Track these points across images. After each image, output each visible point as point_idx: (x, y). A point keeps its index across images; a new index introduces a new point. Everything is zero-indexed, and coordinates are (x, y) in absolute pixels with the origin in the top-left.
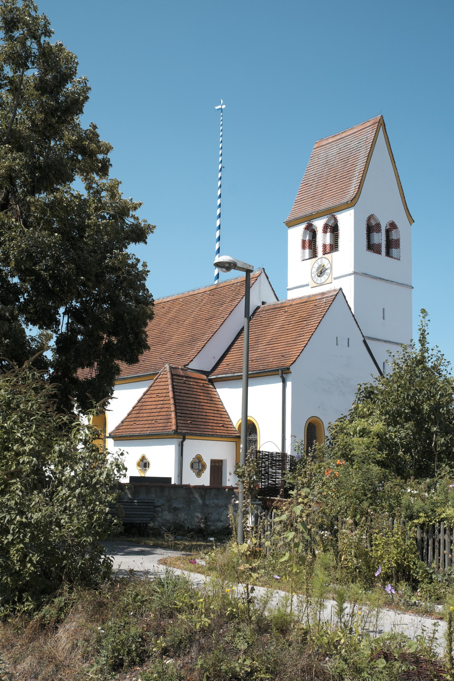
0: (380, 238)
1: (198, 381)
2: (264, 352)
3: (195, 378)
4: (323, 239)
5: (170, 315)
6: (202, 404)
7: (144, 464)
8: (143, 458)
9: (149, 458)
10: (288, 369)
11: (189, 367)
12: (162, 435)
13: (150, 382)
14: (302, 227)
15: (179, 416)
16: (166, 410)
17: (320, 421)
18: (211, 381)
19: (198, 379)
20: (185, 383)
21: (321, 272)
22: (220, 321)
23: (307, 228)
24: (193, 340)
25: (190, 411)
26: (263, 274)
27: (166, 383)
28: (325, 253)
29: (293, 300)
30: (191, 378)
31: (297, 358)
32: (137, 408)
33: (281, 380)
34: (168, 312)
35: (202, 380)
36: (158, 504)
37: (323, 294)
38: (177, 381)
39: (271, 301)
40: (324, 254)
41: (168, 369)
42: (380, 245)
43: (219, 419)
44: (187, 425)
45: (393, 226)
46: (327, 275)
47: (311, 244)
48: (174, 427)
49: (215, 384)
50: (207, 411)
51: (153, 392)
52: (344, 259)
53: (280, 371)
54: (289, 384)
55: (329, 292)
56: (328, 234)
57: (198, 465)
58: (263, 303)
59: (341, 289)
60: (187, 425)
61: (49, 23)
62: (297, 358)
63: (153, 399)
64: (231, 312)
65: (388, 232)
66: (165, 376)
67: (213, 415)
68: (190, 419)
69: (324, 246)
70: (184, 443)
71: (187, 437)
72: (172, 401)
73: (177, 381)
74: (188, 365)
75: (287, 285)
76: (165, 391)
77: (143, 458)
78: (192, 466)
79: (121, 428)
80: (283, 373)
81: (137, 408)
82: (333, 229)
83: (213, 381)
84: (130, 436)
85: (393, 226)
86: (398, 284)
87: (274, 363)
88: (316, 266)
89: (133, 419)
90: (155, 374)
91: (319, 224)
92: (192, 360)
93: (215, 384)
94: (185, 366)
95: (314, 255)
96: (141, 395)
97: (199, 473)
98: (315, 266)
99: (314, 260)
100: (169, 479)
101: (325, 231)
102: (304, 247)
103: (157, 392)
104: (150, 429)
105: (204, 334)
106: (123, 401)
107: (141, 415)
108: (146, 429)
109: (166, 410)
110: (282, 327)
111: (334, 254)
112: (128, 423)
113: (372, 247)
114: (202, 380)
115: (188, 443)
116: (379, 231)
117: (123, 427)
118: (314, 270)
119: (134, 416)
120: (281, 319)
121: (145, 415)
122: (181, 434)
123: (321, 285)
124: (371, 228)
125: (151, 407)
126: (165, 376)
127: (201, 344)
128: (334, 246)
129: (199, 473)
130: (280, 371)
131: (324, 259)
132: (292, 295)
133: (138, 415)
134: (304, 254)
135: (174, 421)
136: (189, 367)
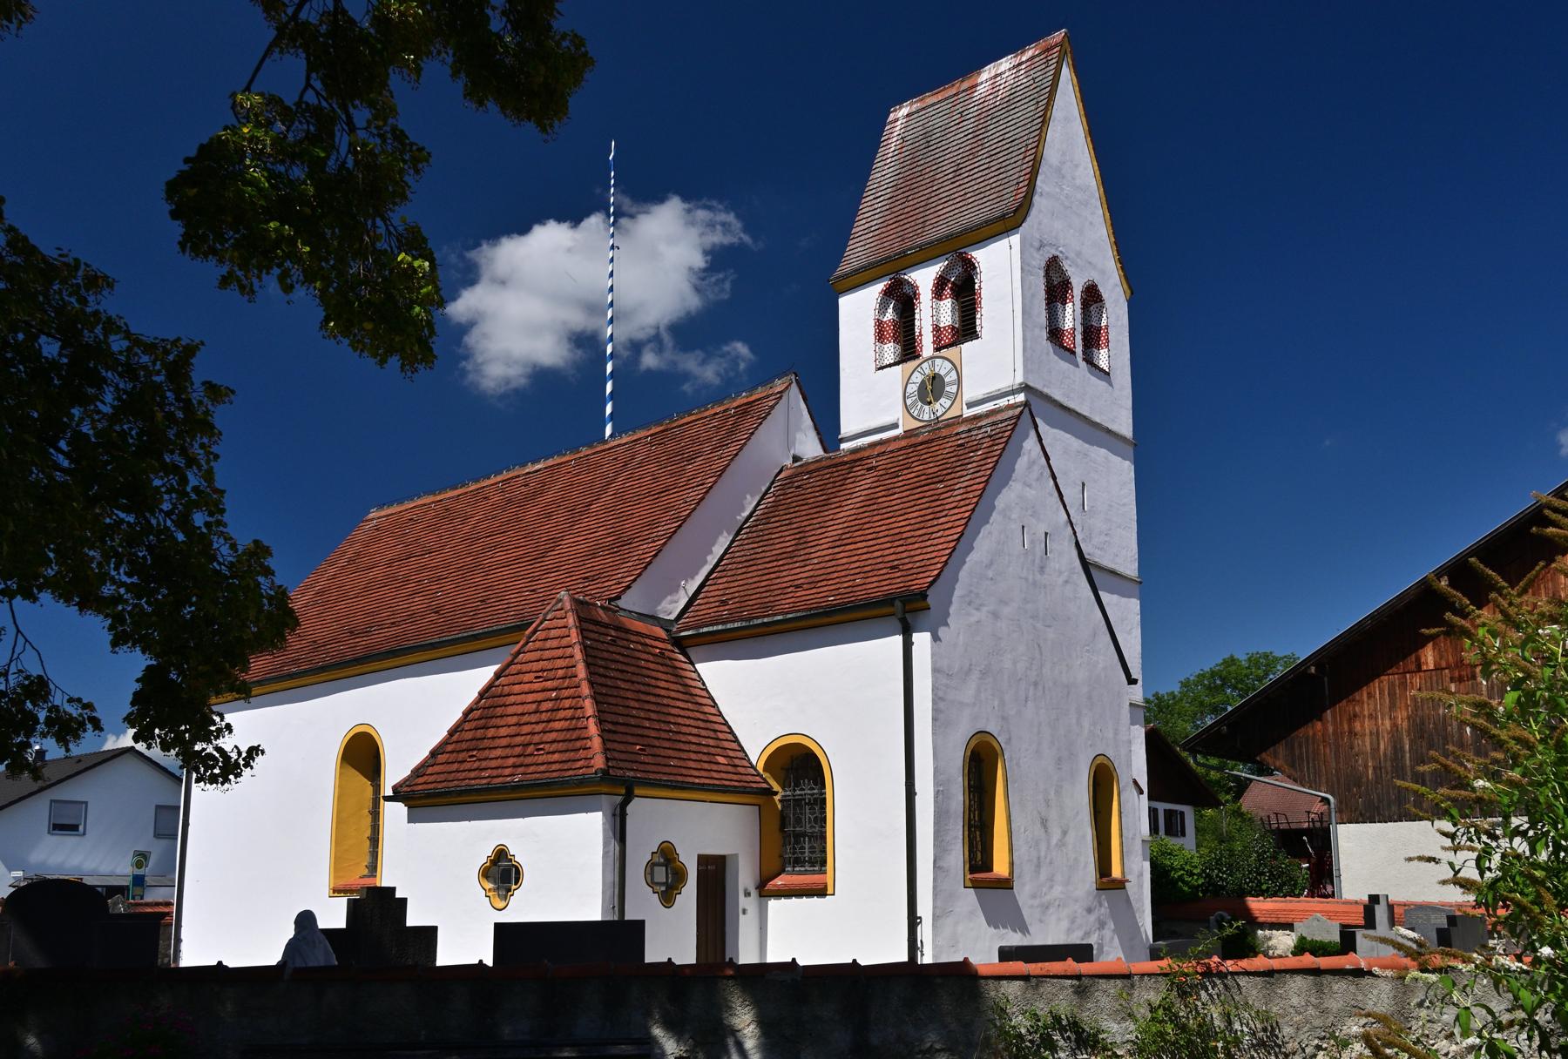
1: (648, 641)
2: (834, 559)
3: (638, 634)
4: (933, 313)
5: (548, 497)
6: (665, 701)
8: (501, 854)
11: (621, 603)
12: (563, 783)
13: (506, 653)
14: (875, 291)
15: (609, 731)
16: (569, 713)
17: (989, 739)
18: (681, 644)
19: (648, 637)
20: (613, 642)
22: (693, 495)
23: (887, 293)
24: (621, 544)
27: (565, 641)
30: (627, 631)
31: (942, 569)
32: (477, 714)
33: (899, 626)
35: (657, 639)
38: (595, 636)
40: (937, 349)
43: (711, 742)
44: (633, 757)
46: (948, 398)
48: (599, 762)
49: (692, 652)
50: (680, 720)
51: (525, 668)
53: (898, 603)
54: (922, 640)
60: (633, 757)
62: (942, 569)
63: (526, 687)
64: (723, 471)
66: (561, 623)
67: (695, 731)
68: (641, 740)
70: (629, 809)
71: (637, 791)
73: (595, 636)
74: (618, 598)
75: (843, 430)
76: (560, 663)
77: (501, 854)
79: (430, 770)
81: (477, 714)
82: (962, 289)
83: (685, 643)
84: (461, 793)
87: (878, 586)
88: (918, 378)
89: (464, 745)
90: (521, 628)
91: (924, 278)
92: (628, 587)
93: (692, 652)
94: (611, 600)
95: (909, 351)
98: (913, 379)
99: (912, 364)
101: (938, 293)
102: (880, 337)
103: (536, 666)
104: (521, 770)
108: (507, 772)
109: (569, 713)
111: (967, 347)
112: (453, 757)
114: (657, 639)
115: (639, 809)
117: (437, 769)
118: (913, 388)
119: (469, 735)
121: (503, 732)
122: (616, 787)
125: (520, 709)
126: (561, 623)
128: (966, 329)
130: (898, 603)
131: (938, 361)
133: (479, 733)
134: (879, 355)
135: (596, 743)
136: (621, 603)
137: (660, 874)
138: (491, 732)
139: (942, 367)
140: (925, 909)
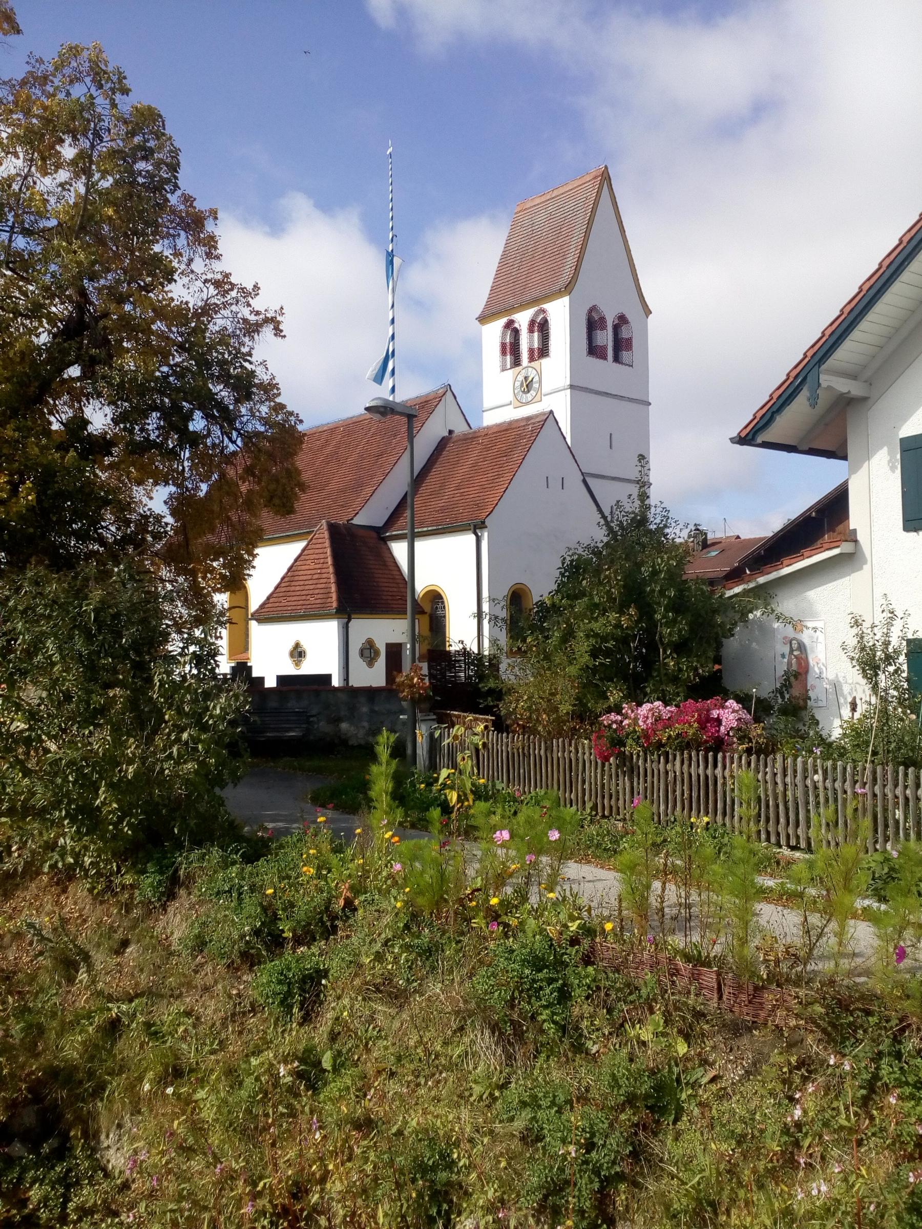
0: (605, 338)
7: (298, 653)
8: (297, 645)
9: (305, 645)
10: (483, 523)
21: (528, 385)
24: (358, 486)
25: (360, 579)
26: (449, 392)
28: (532, 359)
29: (488, 428)
34: (323, 447)
36: (314, 712)
37: (528, 419)
39: (460, 428)
41: (325, 527)
42: (604, 348)
45: (622, 320)
47: (511, 350)
52: (557, 369)
55: (537, 416)
56: (536, 334)
57: (369, 652)
58: (451, 432)
59: (551, 412)
61: (125, 78)
65: (616, 328)
69: (531, 351)
72: (331, 570)
76: (322, 556)
77: (297, 645)
78: (362, 654)
80: (477, 527)
82: (542, 327)
85: (622, 320)
86: (631, 400)
88: (521, 378)
96: (298, 552)
97: (371, 662)
99: (518, 369)
100: (328, 678)
101: (531, 331)
102: (503, 352)
103: (312, 557)
105: (372, 477)
106: (270, 565)
107: (293, 588)
110: (474, 465)
111: (544, 361)
113: (594, 350)
116: (603, 327)
118: (518, 384)
120: (474, 455)
121: (298, 588)
123: (527, 403)
124: (594, 323)
127: (369, 490)
128: (543, 351)
129: (371, 662)
132: (491, 419)
135: (334, 596)
137: (367, 653)
138: (293, 588)
139: (532, 374)
140: (485, 593)
